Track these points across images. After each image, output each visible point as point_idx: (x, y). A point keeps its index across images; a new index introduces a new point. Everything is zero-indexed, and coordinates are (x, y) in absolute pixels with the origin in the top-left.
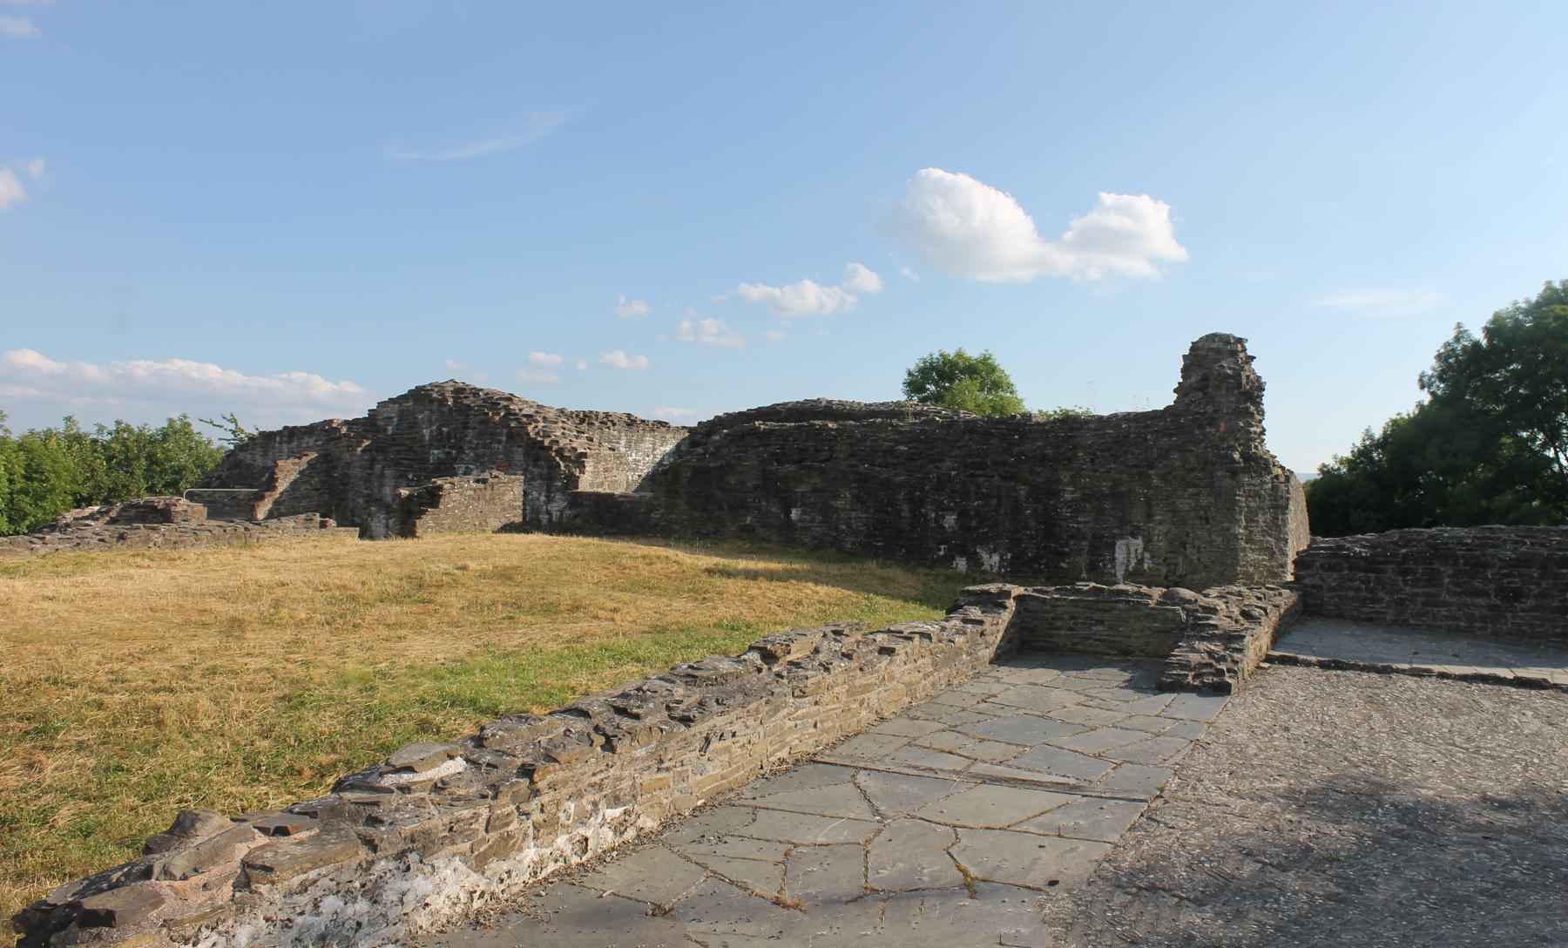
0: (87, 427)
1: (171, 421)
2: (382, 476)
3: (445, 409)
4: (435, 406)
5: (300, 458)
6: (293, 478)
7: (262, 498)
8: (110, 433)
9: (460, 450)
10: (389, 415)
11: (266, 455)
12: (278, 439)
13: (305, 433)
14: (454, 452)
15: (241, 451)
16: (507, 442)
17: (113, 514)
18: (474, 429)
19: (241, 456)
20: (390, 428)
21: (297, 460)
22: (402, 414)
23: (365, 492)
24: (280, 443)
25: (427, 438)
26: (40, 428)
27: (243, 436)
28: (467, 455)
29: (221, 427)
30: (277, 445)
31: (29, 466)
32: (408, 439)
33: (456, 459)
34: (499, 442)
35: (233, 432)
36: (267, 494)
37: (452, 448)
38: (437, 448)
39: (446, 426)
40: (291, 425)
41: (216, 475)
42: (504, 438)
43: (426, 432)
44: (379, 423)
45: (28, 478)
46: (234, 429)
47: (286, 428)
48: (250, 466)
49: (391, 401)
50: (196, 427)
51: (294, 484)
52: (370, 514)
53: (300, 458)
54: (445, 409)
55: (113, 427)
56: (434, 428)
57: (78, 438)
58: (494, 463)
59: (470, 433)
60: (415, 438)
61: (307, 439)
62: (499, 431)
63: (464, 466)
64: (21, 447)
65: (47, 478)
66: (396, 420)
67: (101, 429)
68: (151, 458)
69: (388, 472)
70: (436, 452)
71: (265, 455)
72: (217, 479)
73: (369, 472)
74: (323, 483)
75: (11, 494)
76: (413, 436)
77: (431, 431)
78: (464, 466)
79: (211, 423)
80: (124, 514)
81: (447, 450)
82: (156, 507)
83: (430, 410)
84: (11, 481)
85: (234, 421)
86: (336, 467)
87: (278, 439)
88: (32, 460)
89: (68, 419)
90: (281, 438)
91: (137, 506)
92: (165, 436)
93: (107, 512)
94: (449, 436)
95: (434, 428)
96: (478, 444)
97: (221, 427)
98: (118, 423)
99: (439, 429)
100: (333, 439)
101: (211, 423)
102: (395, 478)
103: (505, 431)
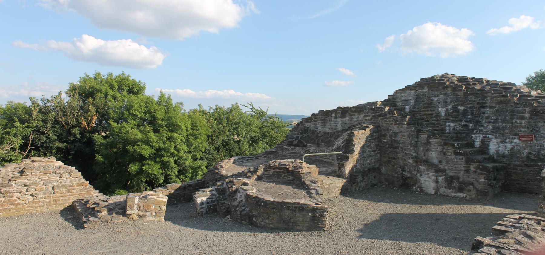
0: (206, 108)
1: (233, 105)
2: (428, 143)
3: (459, 93)
4: (449, 91)
5: (365, 130)
6: (362, 144)
7: (347, 158)
8: (214, 110)
9: (478, 123)
10: (407, 98)
11: (325, 125)
12: (333, 115)
13: (355, 111)
14: (471, 125)
15: (307, 122)
16: (530, 118)
17: (259, 173)
18: (491, 107)
19: (307, 125)
20: (407, 107)
21: (363, 131)
22: (418, 98)
23: (414, 154)
24: (336, 118)
25: (443, 114)
26: (192, 108)
27: (255, 110)
28: (486, 128)
29: (247, 107)
30: (333, 119)
31: (192, 124)
32: (425, 114)
33: (473, 130)
34: (523, 118)
35: (252, 109)
36: (350, 155)
37: (470, 121)
38: (453, 122)
39: (462, 105)
40: (343, 105)
41: (295, 137)
42: (527, 115)
43: (442, 111)
44: (398, 104)
45: (192, 129)
46: (252, 108)
47: (339, 108)
48: (313, 132)
49: (408, 88)
50: (241, 107)
51: (363, 148)
52: (419, 171)
53: (365, 130)
54: (459, 93)
55: (214, 108)
56: (450, 107)
57: (204, 112)
58: (516, 134)
59: (488, 111)
60: (432, 114)
61: (357, 115)
62: (520, 109)
63: (481, 136)
64: (190, 117)
65: (198, 129)
66: (412, 102)
67: (210, 108)
68: (228, 119)
69: (433, 141)
70: (452, 124)
71: (324, 125)
72: (296, 139)
73: (416, 140)
74: (377, 146)
75: (187, 135)
76: (430, 112)
77: (447, 110)
78: (481, 136)
79: (244, 105)
80: (266, 173)
81: (463, 123)
82: (288, 169)
83: (445, 94)
84: (187, 130)
85: (252, 105)
86: (385, 135)
87: (333, 115)
88: (193, 121)
89: (200, 105)
90: (336, 115)
91: (274, 168)
92: (231, 111)
93: (255, 171)
94: (465, 113)
95: (450, 107)
96: (497, 119)
97: (247, 107)
98: (216, 106)
99: (455, 108)
100: (380, 116)
101: (244, 105)
102: (441, 145)
103: (527, 109)
